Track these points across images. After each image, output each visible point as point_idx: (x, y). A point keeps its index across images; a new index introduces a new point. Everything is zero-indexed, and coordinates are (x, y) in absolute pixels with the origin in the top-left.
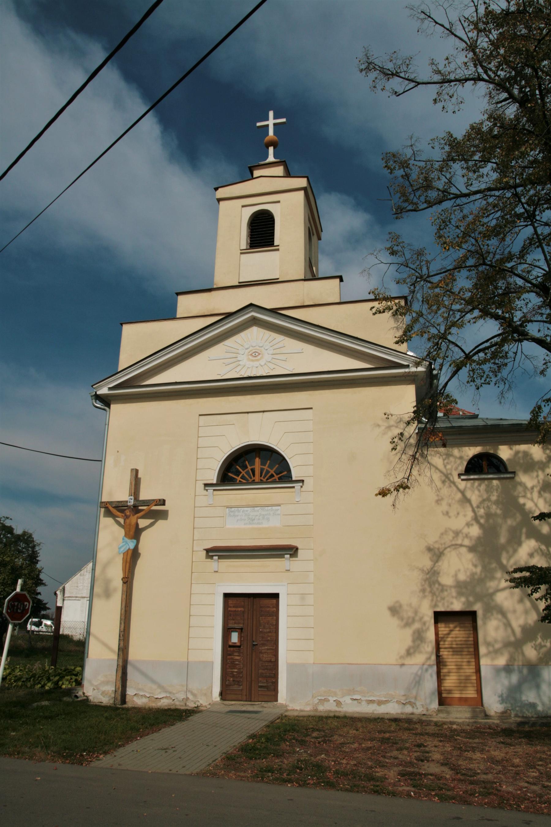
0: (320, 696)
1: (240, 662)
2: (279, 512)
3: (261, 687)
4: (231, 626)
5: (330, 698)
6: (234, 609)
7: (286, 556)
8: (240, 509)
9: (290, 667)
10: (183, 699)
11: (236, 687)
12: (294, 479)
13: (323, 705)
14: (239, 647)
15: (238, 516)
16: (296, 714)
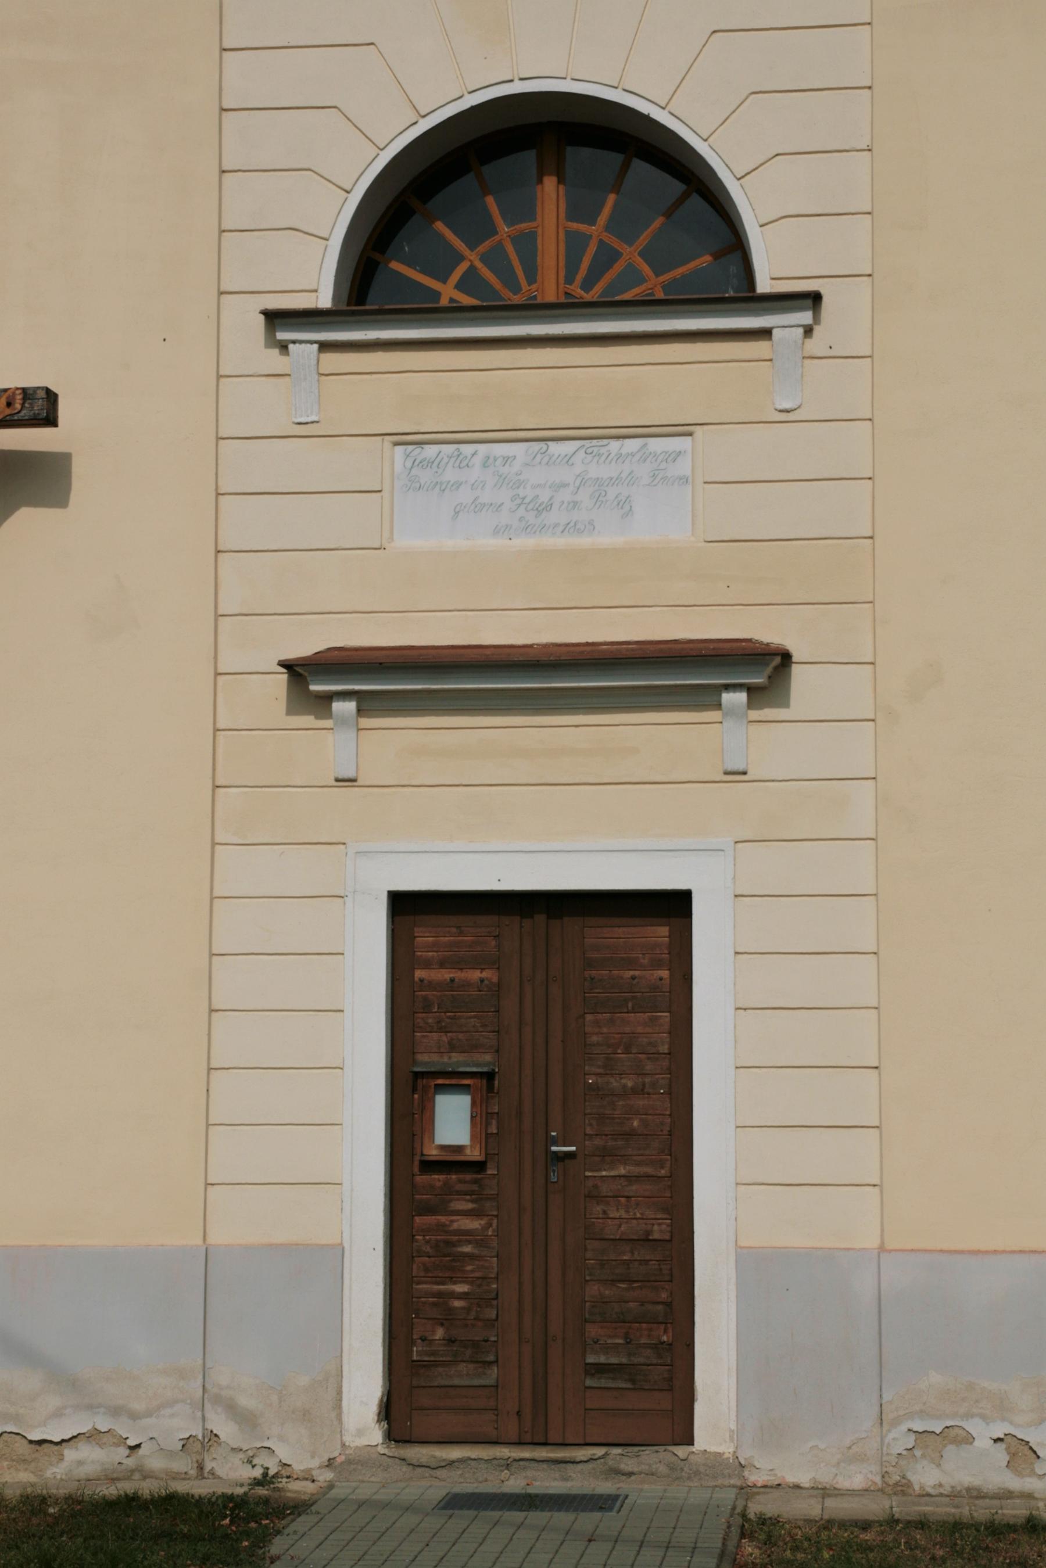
0: (922, 1414)
1: (481, 1243)
2: (684, 467)
3: (599, 1370)
4: (428, 1060)
5: (974, 1426)
6: (446, 975)
7: (728, 698)
8: (467, 449)
9: (753, 1265)
10: (186, 1443)
11: (462, 1375)
12: (764, 285)
13: (938, 1462)
14: (479, 1166)
15: (458, 485)
16: (812, 1508)
